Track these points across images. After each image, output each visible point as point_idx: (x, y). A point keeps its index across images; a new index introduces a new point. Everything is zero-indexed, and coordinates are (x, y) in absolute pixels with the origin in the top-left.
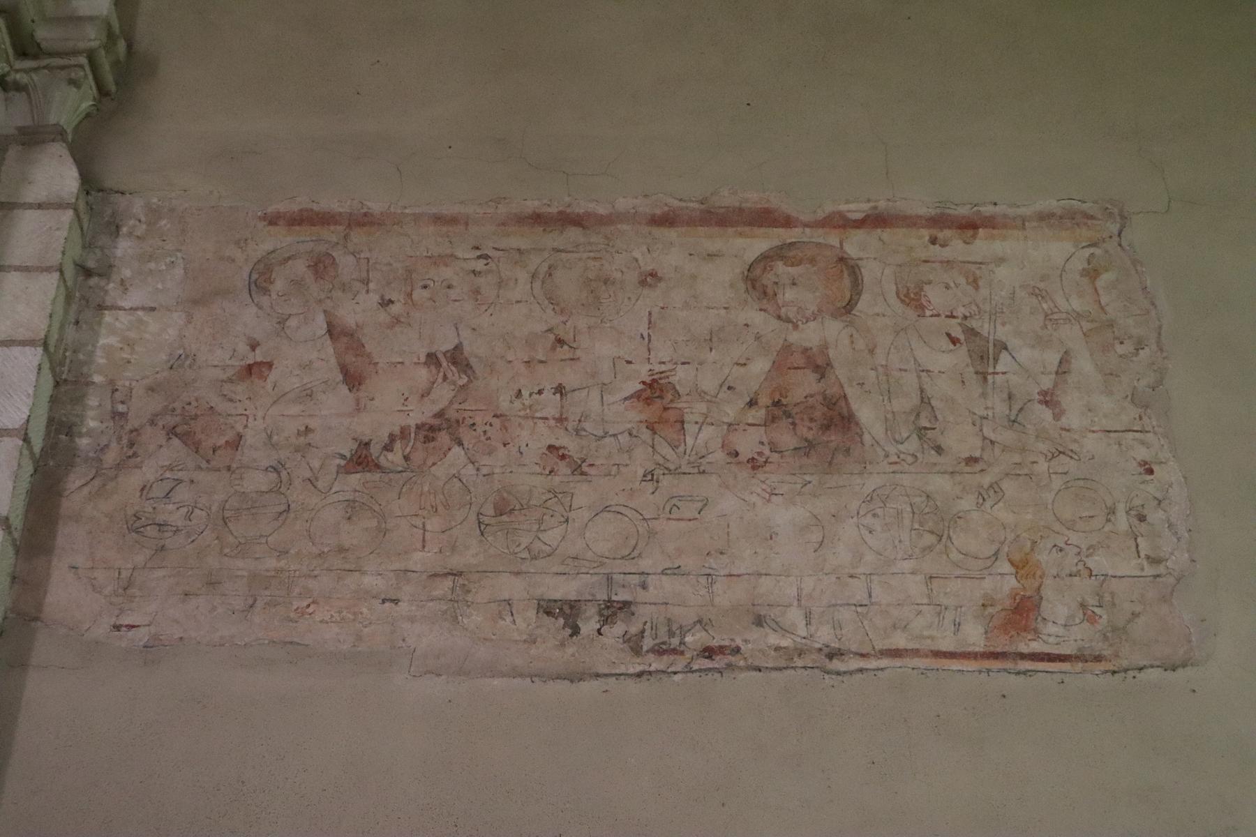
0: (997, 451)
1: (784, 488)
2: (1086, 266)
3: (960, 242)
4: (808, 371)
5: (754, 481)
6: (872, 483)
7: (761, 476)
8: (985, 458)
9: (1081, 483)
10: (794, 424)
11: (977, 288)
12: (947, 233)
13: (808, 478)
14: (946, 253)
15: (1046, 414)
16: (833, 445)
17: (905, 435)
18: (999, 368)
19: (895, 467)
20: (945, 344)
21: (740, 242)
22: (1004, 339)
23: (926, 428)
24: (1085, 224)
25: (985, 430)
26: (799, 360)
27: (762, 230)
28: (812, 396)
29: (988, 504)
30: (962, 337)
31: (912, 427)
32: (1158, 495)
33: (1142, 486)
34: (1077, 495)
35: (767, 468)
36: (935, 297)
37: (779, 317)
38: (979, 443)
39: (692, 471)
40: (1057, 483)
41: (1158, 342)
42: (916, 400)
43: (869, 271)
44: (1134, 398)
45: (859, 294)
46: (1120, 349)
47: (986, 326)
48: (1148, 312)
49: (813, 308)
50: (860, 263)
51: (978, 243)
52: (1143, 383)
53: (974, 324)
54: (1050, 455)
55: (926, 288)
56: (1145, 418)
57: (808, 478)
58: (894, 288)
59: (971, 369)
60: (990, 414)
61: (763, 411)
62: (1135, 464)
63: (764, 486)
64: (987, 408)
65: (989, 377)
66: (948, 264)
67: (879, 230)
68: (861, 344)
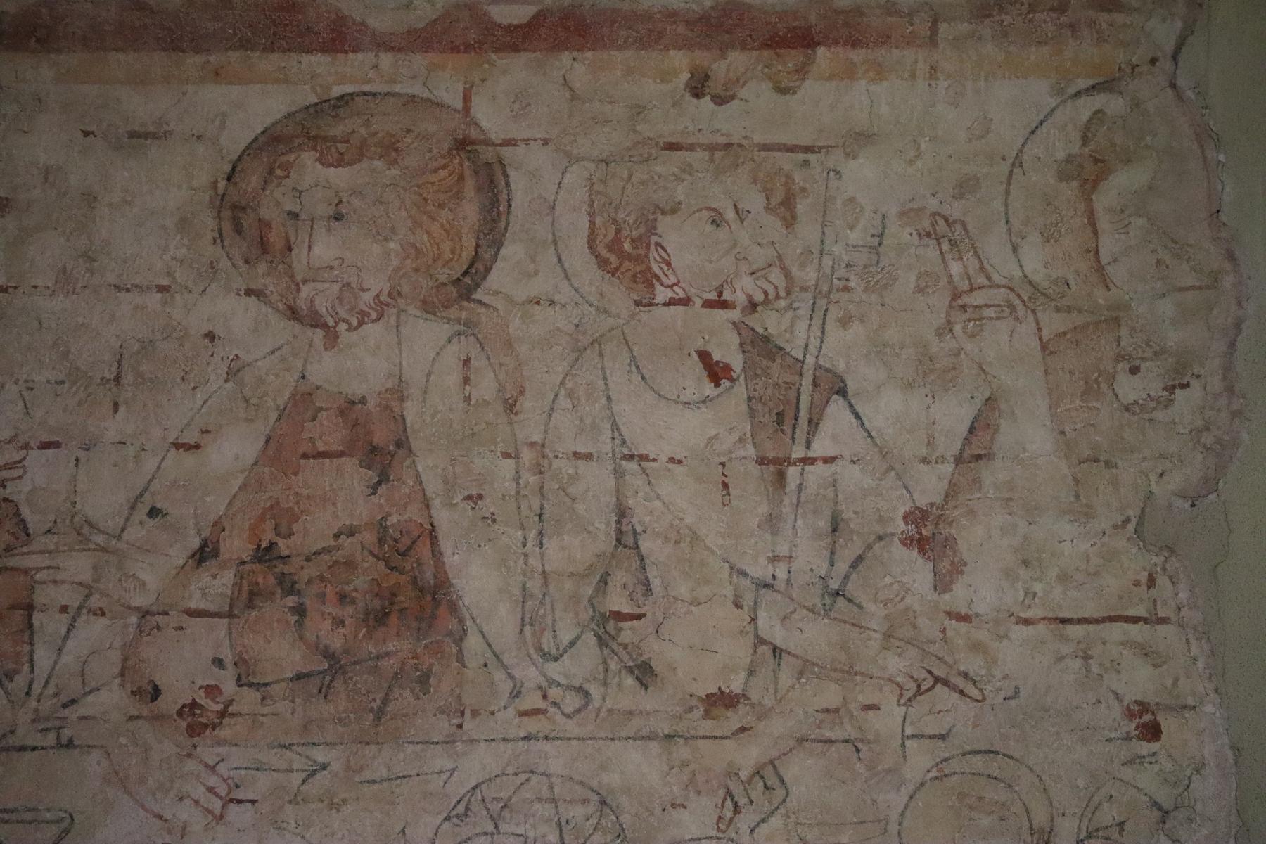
0: (786, 678)
1: (261, 785)
2: (1076, 148)
3: (766, 86)
4: (349, 464)
5: (191, 765)
6: (479, 763)
7: (208, 753)
8: (754, 696)
9: (978, 762)
10: (300, 611)
11: (790, 221)
12: (738, 60)
13: (320, 755)
14: (727, 122)
15: (917, 573)
16: (389, 665)
17: (565, 638)
18: (820, 447)
19: (532, 725)
20: (696, 384)
21: (214, 96)
22: (841, 366)
23: (619, 616)
24: (1092, 24)
25: (762, 615)
26: (329, 432)
27: (276, 58)
28: (351, 532)
29: (746, 820)
30: (737, 362)
31: (586, 615)
32: (1164, 797)
33: (1127, 774)
34: (962, 796)
35: (224, 733)
36: (686, 250)
37: (293, 313)
38: (742, 653)
39: (38, 740)
40: (919, 761)
41: (1227, 369)
42: (604, 540)
43: (531, 178)
44: (1141, 527)
45: (498, 244)
46: (1129, 389)
47: (801, 329)
48: (1216, 276)
49: (376, 284)
50: (506, 152)
51: (811, 89)
52: (1176, 480)
53: (770, 322)
54: (912, 686)
55: (664, 223)
56: (1162, 580)
57: (320, 755)
58: (584, 223)
59: (750, 451)
60: (781, 573)
61: (228, 577)
62: (1117, 711)
63: (213, 781)
64: (775, 559)
65: (792, 472)
66: (727, 152)
67: (566, 57)
68: (486, 387)
